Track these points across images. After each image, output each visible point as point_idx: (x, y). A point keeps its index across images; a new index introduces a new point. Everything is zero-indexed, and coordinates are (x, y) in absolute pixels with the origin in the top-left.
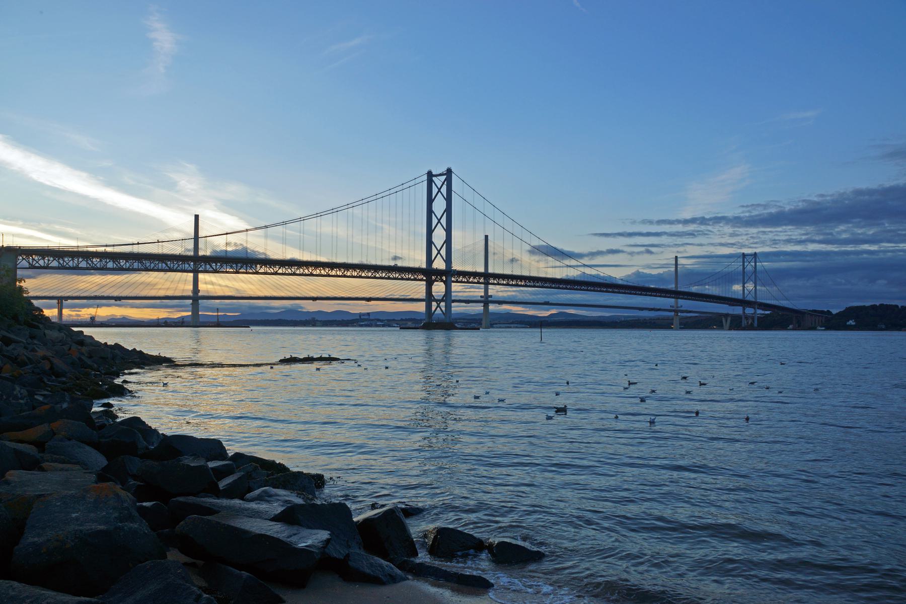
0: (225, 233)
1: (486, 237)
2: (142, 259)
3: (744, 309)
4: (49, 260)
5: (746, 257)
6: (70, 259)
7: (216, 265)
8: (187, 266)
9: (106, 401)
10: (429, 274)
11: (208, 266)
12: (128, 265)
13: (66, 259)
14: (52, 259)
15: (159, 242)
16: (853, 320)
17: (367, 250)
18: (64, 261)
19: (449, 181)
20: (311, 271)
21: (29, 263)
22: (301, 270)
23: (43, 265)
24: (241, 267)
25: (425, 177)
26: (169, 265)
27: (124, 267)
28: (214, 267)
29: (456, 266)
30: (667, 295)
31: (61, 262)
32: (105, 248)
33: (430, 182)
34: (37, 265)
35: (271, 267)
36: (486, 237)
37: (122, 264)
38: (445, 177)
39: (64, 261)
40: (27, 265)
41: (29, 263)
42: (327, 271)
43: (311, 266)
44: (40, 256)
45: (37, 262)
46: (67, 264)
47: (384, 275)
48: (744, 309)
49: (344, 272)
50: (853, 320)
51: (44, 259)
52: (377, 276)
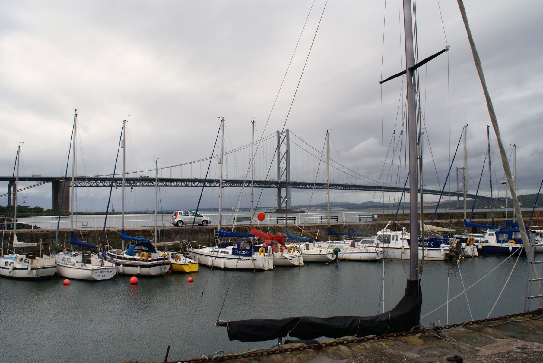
0: (157, 162)
1: (169, 347)
2: (152, 181)
3: (458, 198)
4: (98, 183)
5: (459, 169)
6: (108, 182)
7: (196, 183)
8: (173, 183)
9: (176, 227)
10: (280, 185)
11: (183, 184)
12: (146, 184)
13: (106, 182)
14: (100, 182)
15: (136, 172)
16: (520, 202)
17: (75, 126)
18: (105, 183)
19: (287, 136)
20: (232, 184)
21: (90, 184)
22: (235, 184)
23: (96, 185)
24: (189, 183)
25: (276, 134)
26: (165, 183)
27: (144, 185)
28: (185, 184)
29: (294, 178)
30: (392, 190)
31: (104, 183)
32: (111, 176)
33: (279, 138)
34: (107, 185)
35: (212, 183)
36: (169, 347)
37: (143, 183)
38: (462, 169)
39: (105, 183)
40: (89, 185)
41: (90, 184)
42: (240, 184)
43: (232, 182)
44: (95, 181)
45: (93, 184)
46: (107, 184)
47: (268, 185)
48: (458, 198)
49: (256, 185)
50: (520, 202)
51: (96, 182)
52: (272, 186)
